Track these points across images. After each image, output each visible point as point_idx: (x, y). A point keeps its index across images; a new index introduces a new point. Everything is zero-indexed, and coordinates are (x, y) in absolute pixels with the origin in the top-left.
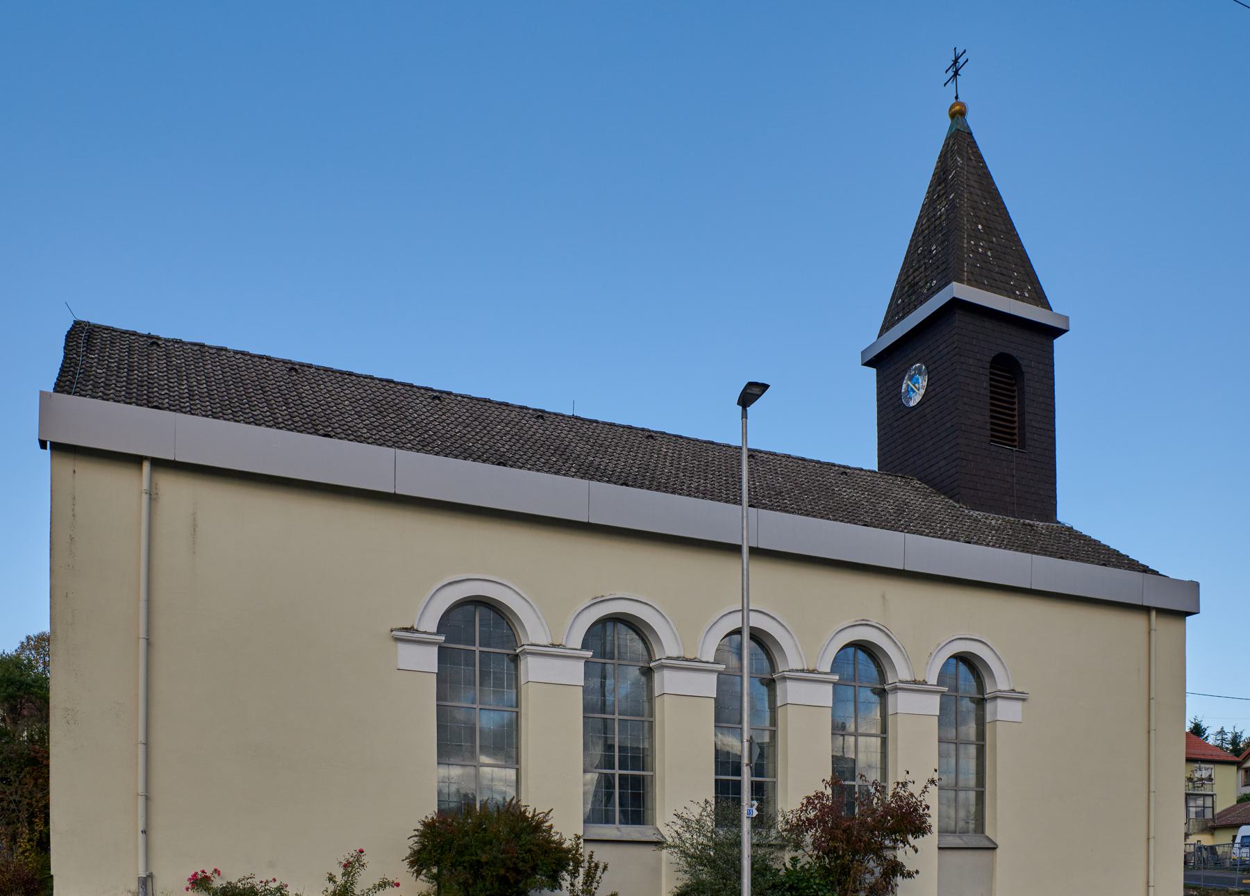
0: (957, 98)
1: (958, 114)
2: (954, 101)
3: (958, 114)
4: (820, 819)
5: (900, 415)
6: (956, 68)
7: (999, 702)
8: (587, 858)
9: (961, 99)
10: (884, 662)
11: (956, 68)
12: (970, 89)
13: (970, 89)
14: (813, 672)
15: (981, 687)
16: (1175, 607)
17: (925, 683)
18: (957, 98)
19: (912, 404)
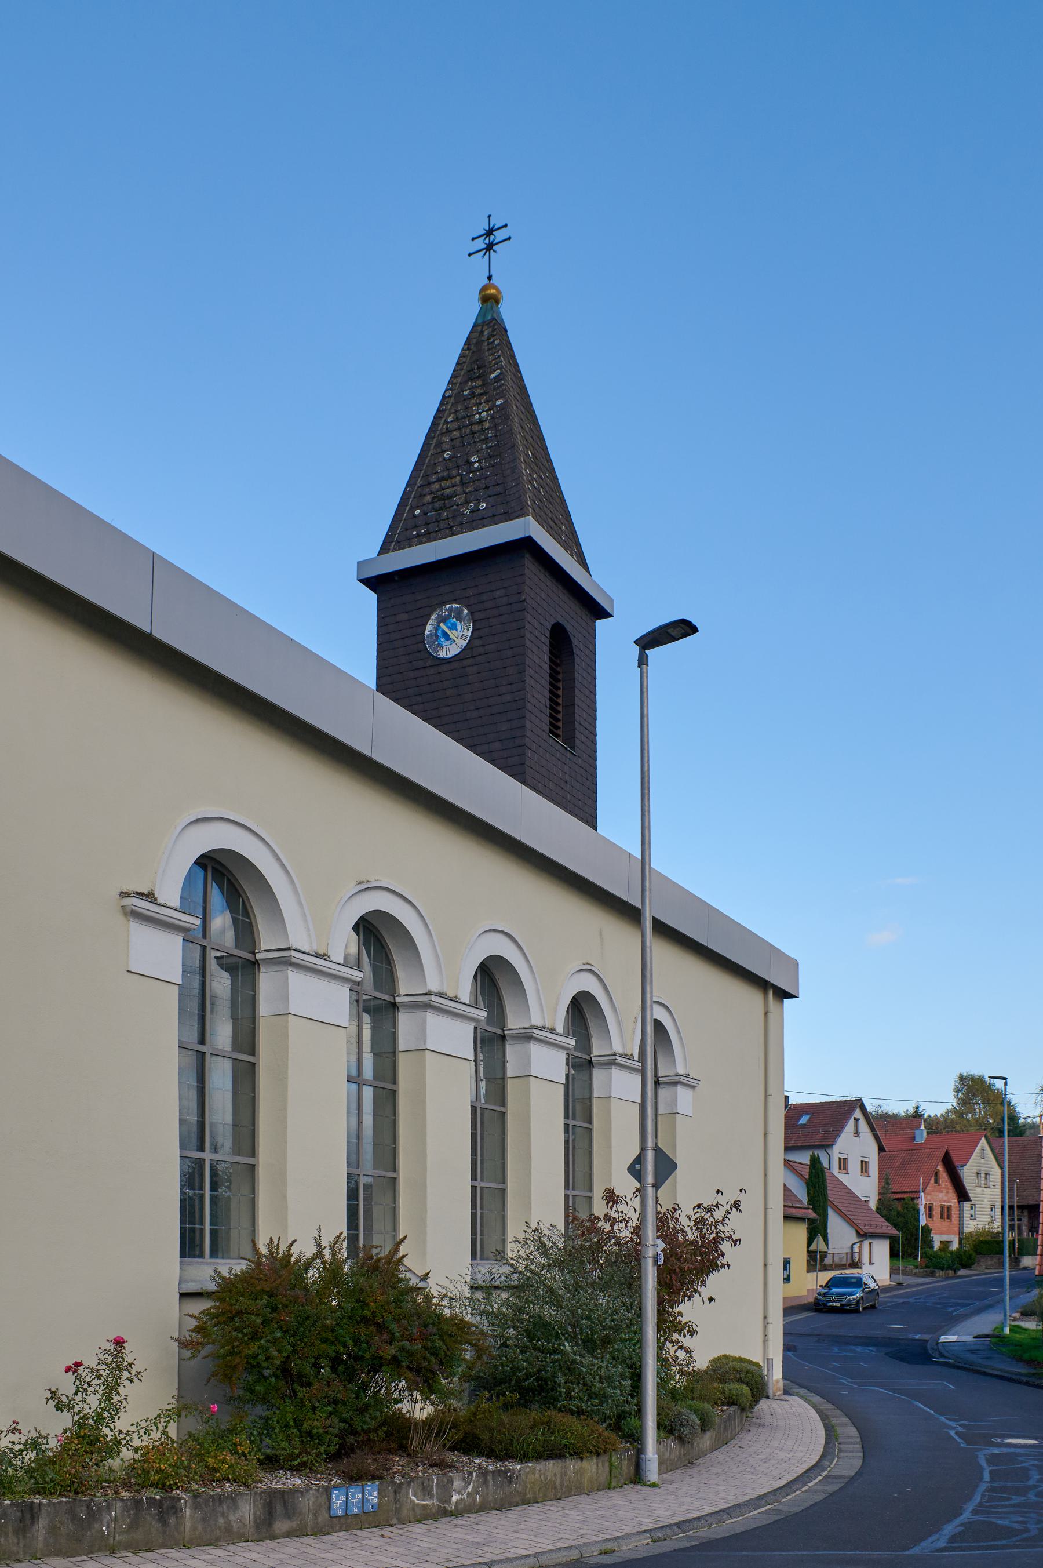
0: (489, 278)
1: (489, 299)
2: (485, 281)
3: (489, 299)
4: (517, 1289)
5: (421, 664)
6: (489, 240)
7: (615, 1072)
8: (106, 1356)
9: (495, 281)
10: (592, 1023)
11: (489, 240)
12: (507, 269)
13: (507, 269)
14: (323, 956)
15: (245, 930)
16: (769, 987)
17: (150, 897)
18: (489, 278)
19: (443, 654)
